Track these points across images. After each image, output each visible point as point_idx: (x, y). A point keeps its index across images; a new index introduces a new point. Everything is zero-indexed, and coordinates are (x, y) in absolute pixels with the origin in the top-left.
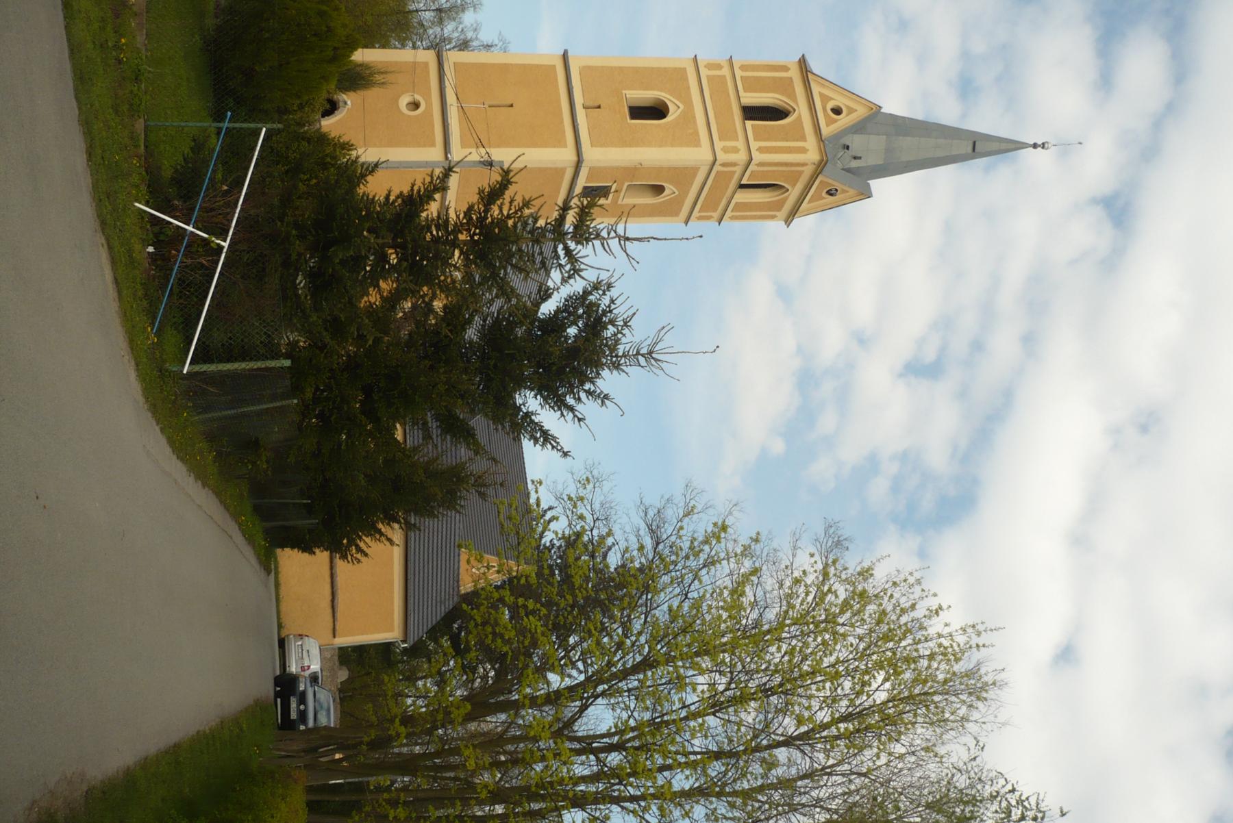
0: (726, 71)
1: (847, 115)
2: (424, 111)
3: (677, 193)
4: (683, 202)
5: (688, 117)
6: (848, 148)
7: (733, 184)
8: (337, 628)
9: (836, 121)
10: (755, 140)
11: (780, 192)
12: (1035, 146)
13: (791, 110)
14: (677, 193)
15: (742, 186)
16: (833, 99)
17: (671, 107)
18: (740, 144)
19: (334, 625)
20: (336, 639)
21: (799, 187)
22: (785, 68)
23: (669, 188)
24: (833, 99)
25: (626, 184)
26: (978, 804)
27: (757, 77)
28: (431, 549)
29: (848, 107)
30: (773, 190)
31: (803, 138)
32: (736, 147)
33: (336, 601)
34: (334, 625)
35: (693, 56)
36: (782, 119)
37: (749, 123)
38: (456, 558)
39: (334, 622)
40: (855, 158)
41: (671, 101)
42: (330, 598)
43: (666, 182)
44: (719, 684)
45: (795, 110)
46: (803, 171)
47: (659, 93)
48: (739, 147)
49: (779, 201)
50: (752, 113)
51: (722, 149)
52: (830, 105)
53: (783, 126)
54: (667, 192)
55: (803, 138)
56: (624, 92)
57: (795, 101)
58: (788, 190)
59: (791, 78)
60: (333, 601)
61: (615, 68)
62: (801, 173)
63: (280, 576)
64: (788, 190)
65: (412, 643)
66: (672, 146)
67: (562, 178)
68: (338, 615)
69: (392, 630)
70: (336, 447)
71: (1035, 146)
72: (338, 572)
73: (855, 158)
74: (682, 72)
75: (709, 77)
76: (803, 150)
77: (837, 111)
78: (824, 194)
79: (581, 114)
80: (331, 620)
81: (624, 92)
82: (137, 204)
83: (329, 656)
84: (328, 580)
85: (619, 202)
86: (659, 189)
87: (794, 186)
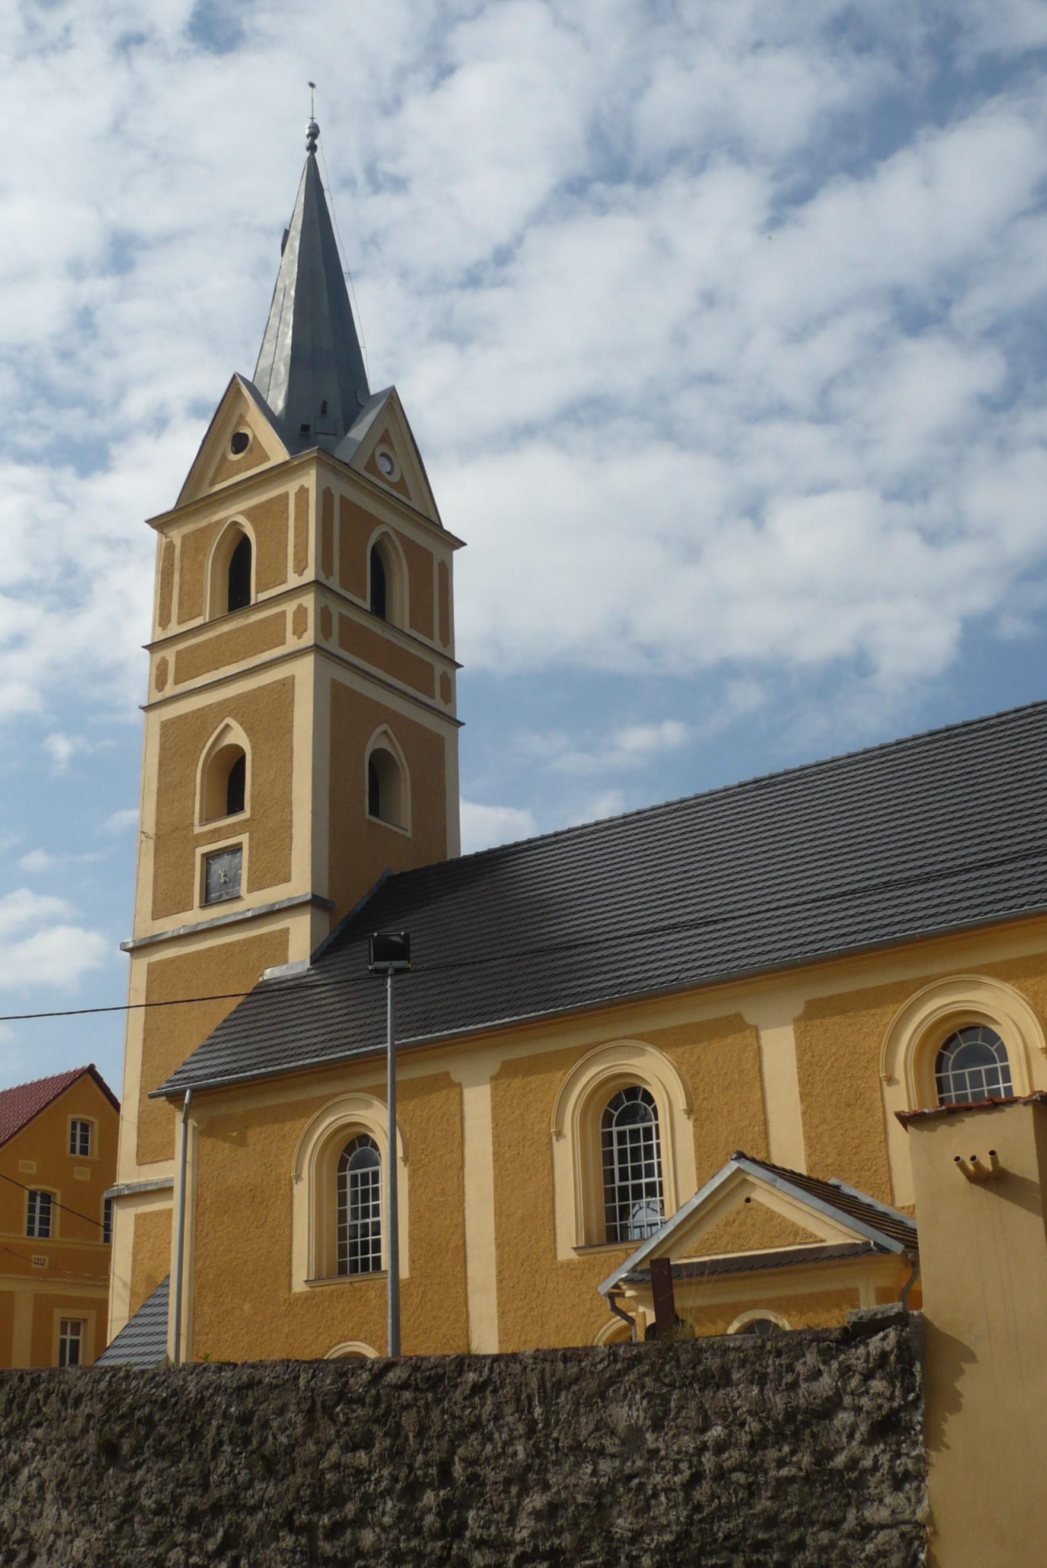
0: (170, 654)
6: (305, 428)
7: (372, 625)
10: (285, 582)
11: (390, 547)
12: (312, 148)
18: (290, 608)
22: (169, 548)
23: (376, 741)
26: (459, 1380)
35: (142, 711)
40: (324, 411)
44: (586, 1441)
46: (342, 498)
48: (297, 489)
51: (300, 575)
54: (384, 744)
57: (218, 523)
70: (317, 1491)
71: (312, 148)
73: (324, 411)
76: (303, 492)
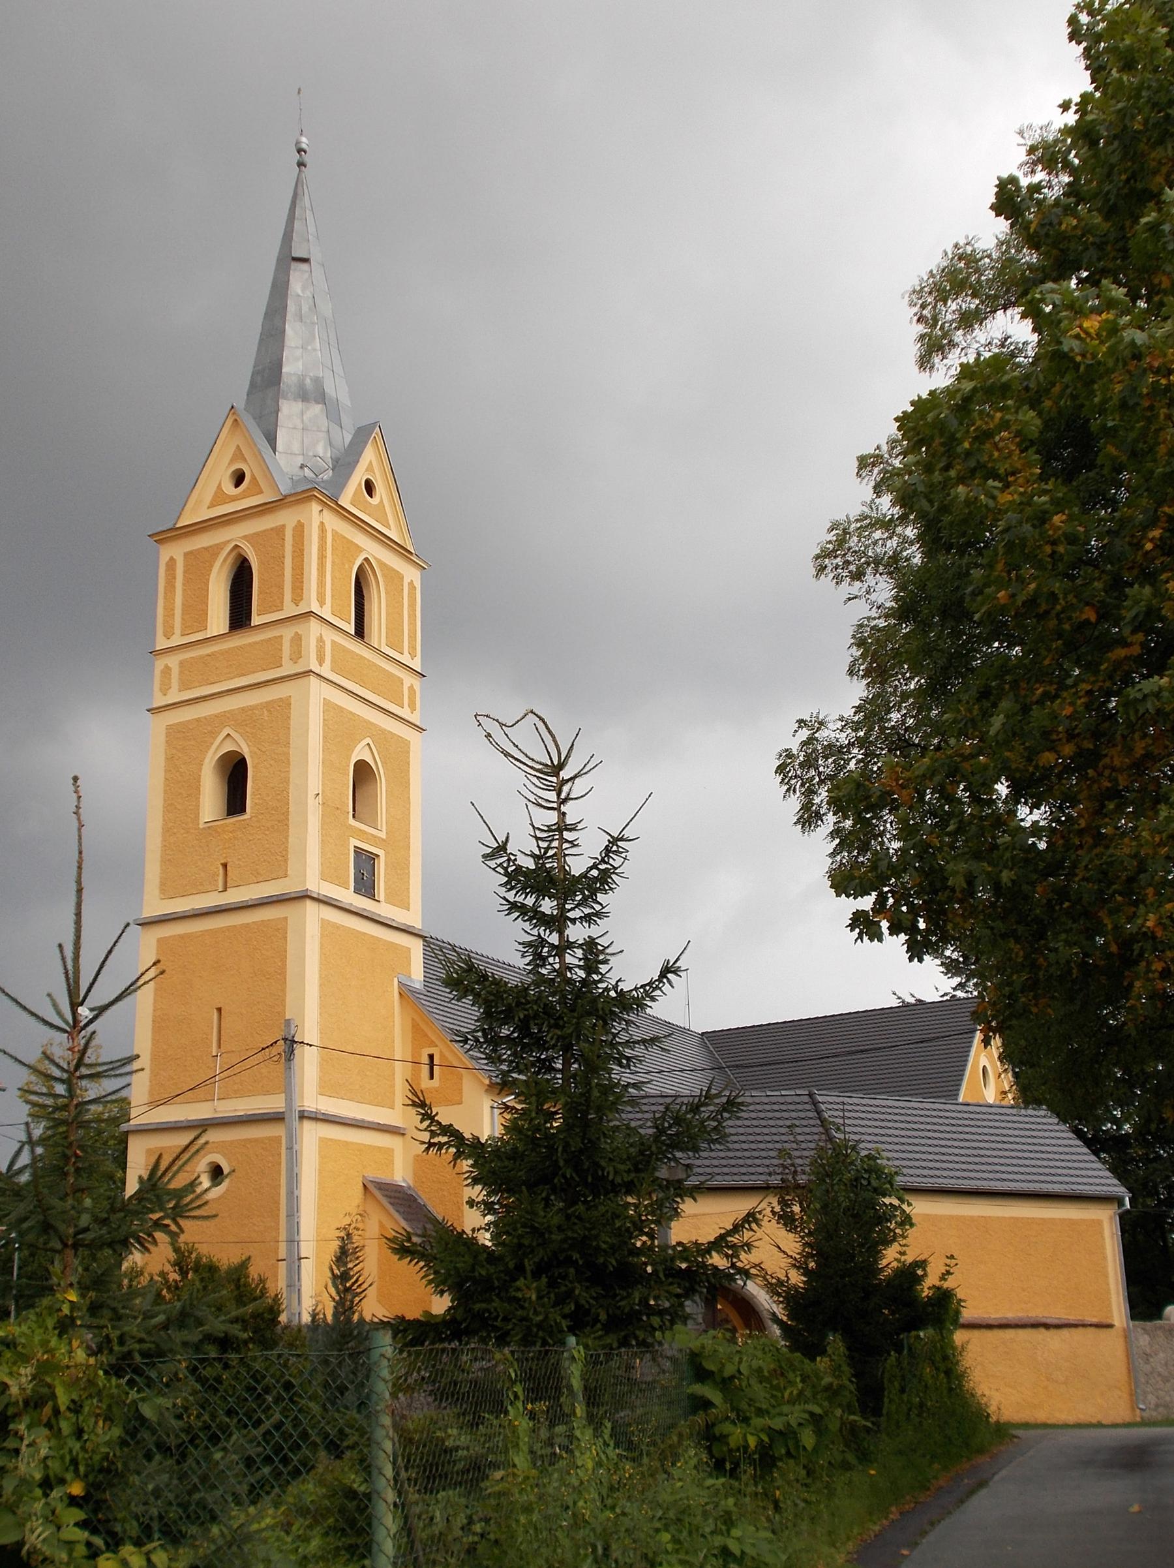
1: (245, 460)
2: (224, 1155)
3: (368, 740)
4: (383, 731)
5: (245, 720)
7: (355, 646)
8: (1095, 1320)
9: (254, 478)
13: (234, 554)
14: (368, 740)
15: (360, 632)
16: (220, 485)
17: (228, 747)
19: (1091, 1325)
20: (1116, 1323)
21: (361, 539)
23: (360, 752)
24: (220, 485)
25: (351, 821)
27: (183, 610)
28: (1033, 1127)
29: (232, 461)
30: (368, 586)
31: (280, 531)
32: (292, 640)
33: (1049, 1321)
34: (1091, 1325)
36: (250, 567)
37: (256, 620)
38: (971, 1108)
39: (1084, 1326)
41: (219, 746)
42: (1042, 1330)
43: (349, 758)
45: (237, 546)
47: (207, 760)
49: (384, 575)
50: (240, 616)
52: (229, 488)
53: (261, 562)
55: (280, 531)
56: (201, 826)
57: (219, 547)
58: (366, 559)
59: (186, 554)
60: (1047, 1326)
61: (164, 840)
62: (335, 533)
63: (1049, 1422)
64: (366, 559)
65: (1123, 1189)
66: (287, 744)
67: (337, 927)
68: (1072, 1318)
69: (1099, 1223)
72: (998, 1316)
74: (175, 734)
75: (184, 686)
77: (239, 478)
78: (374, 501)
79: (235, 896)
80: (1081, 1330)
81: (201, 826)
82: (524, 1078)
83: (1146, 1337)
84: (1009, 1334)
85: (383, 835)
86: (363, 772)
87: (360, 550)
